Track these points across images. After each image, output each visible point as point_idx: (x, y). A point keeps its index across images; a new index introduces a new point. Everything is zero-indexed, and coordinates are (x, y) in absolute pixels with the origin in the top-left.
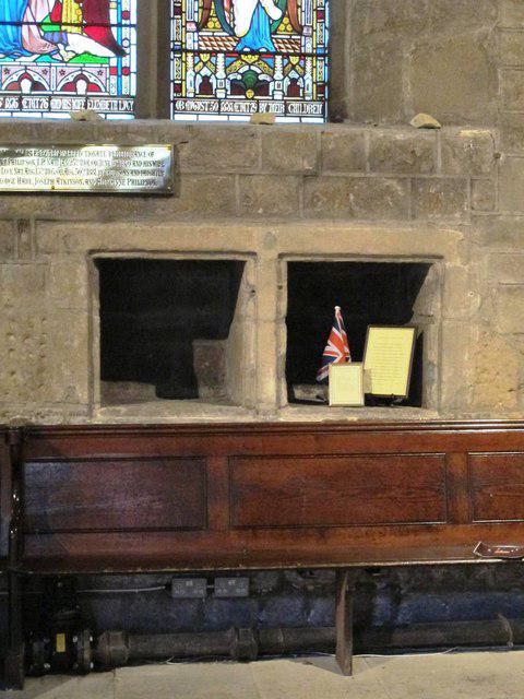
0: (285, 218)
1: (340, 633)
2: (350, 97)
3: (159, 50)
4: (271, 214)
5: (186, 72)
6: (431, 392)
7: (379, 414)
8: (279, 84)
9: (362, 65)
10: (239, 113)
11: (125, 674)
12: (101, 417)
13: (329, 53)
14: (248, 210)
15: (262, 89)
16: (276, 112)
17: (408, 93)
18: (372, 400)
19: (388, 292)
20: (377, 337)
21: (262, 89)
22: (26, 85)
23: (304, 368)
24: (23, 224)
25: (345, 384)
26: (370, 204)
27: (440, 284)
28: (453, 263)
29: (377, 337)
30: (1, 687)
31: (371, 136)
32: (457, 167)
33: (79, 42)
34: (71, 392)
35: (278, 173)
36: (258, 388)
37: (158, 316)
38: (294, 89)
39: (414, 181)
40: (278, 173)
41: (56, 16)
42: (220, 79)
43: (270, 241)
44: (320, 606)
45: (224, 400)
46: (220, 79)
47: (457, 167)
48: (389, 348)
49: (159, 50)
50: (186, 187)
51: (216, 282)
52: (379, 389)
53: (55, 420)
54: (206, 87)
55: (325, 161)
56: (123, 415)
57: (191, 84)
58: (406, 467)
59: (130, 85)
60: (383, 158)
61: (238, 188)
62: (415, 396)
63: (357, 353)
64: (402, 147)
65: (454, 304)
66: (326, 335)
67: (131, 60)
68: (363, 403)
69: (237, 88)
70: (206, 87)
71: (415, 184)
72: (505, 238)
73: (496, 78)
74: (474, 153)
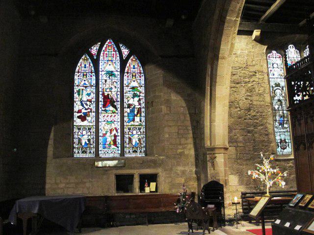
0: (139, 169)
1: (147, 222)
2: (148, 153)
3: (123, 147)
4: (137, 169)
5: (126, 150)
6: (158, 191)
7: (151, 193)
8: (139, 151)
9: (149, 148)
10: (134, 155)
11: (119, 227)
12: (116, 195)
13: (145, 147)
14: (134, 168)
15: (137, 152)
16: (138, 155)
17: (155, 152)
18: (151, 192)
19: (153, 178)
20: (151, 184)
21: (137, 152)
22: (106, 152)
23: (142, 189)
24: (107, 171)
25: (147, 190)
26: (149, 167)
27: (159, 176)
28: (160, 174)
29: (151, 184)
30: (286, 1)
31: (149, 158)
32: (160, 162)
33: (113, 147)
34: (113, 192)
35: (138, 163)
36: (137, 191)
37: (123, 182)
38: (141, 152)
39: (155, 164)
40: (138, 163)
41: (110, 143)
42: (131, 151)
43: (137, 172)
44: (144, 219)
45: (132, 192)
46: (131, 151)
47: (160, 162)
48: (153, 185)
49: (123, 147)
50: (127, 165)
51: (131, 177)
52: (152, 190)
53: (111, 195)
54: (129, 152)
55: (143, 162)
56: (119, 194)
57: (77, 152)
58: (155, 198)
59: (119, 152)
60: (152, 161)
61: (133, 165)
62: (156, 191)
63: (149, 186)
64: (153, 160)
65: (161, 178)
66: (145, 184)
67: (120, 149)
68: (155, 183)
69: (133, 152)
70: (129, 152)
71: (155, 164)
72: (167, 170)
73: (164, 212)
74: (162, 160)
